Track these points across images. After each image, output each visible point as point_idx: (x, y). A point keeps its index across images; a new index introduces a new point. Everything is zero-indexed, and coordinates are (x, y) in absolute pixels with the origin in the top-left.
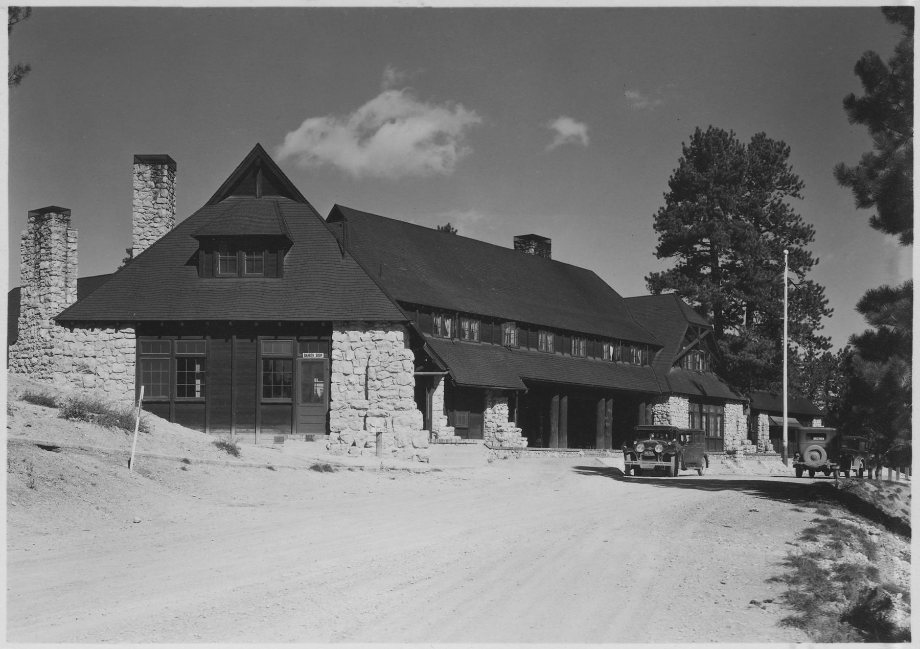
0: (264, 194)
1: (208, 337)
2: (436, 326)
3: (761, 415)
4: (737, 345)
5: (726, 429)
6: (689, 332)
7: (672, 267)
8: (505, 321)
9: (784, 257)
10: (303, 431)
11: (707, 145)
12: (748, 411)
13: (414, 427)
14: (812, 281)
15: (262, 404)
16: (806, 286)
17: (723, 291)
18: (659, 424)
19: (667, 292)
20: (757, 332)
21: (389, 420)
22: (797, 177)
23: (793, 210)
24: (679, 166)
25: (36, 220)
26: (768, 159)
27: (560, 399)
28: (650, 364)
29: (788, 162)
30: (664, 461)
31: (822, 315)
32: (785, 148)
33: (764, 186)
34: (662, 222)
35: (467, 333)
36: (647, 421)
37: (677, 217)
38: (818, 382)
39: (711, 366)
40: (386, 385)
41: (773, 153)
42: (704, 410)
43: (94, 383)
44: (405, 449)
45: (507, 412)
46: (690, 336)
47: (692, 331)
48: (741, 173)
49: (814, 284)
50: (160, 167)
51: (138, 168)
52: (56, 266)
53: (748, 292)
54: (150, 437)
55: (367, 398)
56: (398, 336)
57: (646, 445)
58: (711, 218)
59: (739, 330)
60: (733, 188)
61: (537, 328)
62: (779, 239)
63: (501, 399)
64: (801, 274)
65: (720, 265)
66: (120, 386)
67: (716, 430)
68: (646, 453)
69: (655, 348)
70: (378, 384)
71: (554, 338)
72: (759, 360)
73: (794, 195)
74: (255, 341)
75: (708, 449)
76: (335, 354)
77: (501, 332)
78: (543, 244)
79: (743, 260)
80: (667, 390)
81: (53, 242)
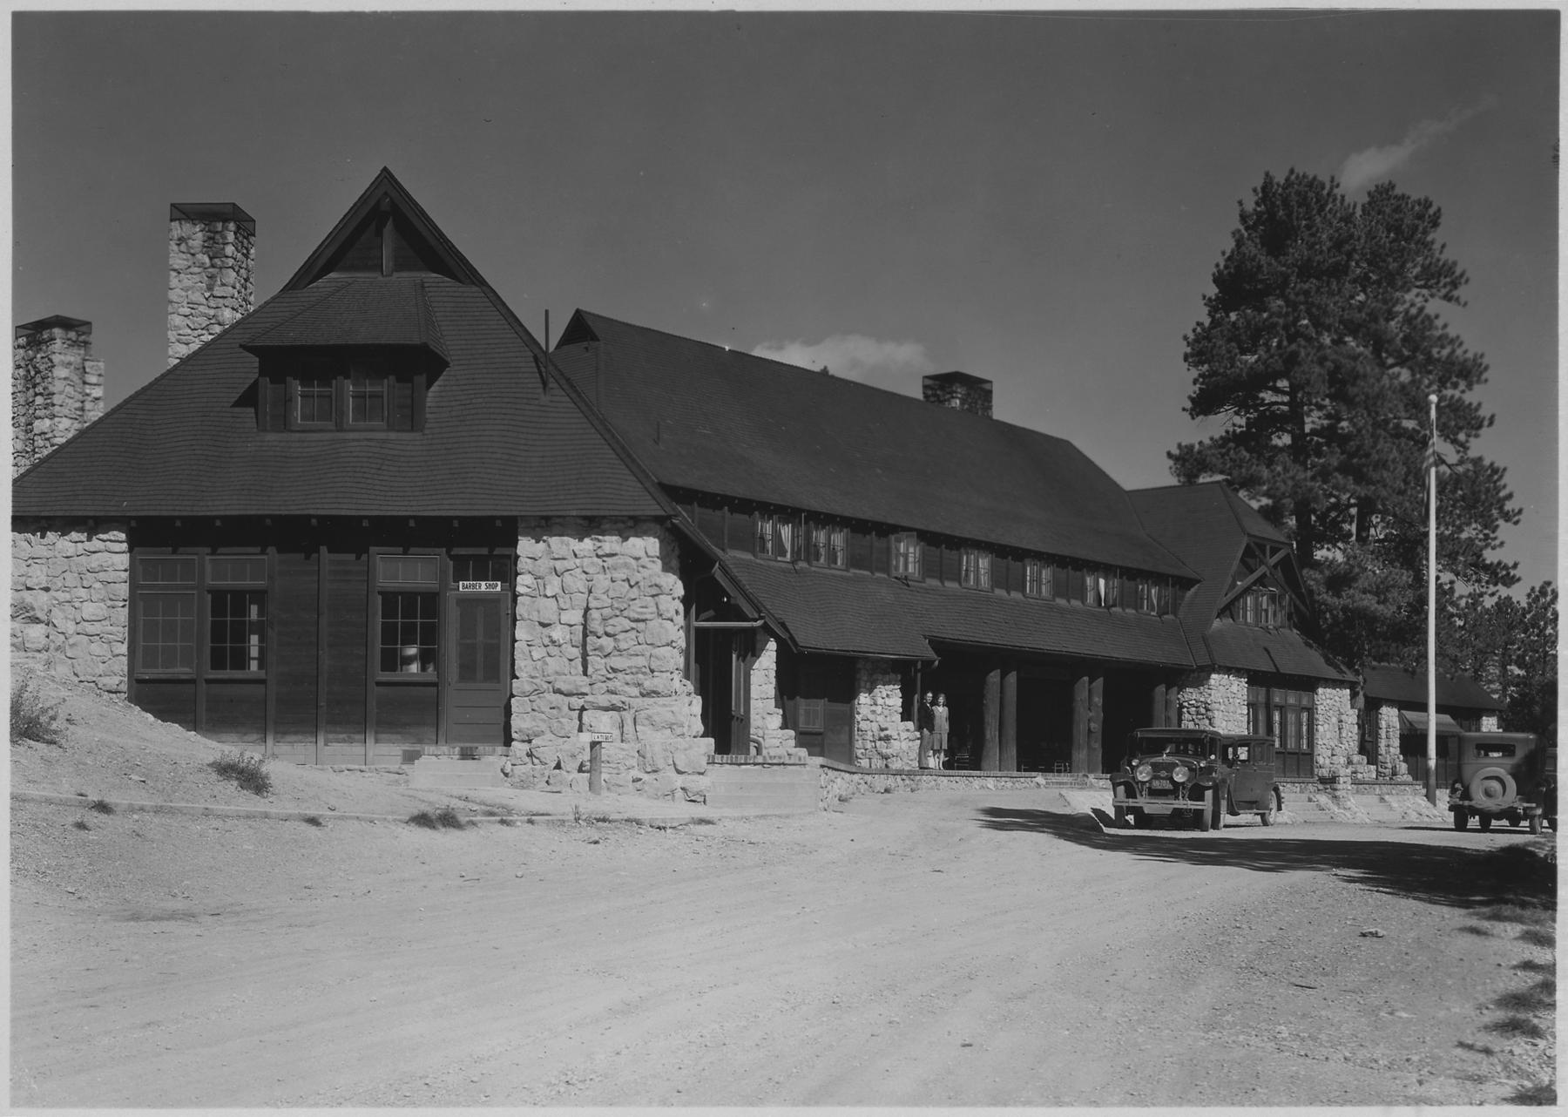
0: (400, 266)
1: (271, 550)
2: (762, 538)
3: (1384, 710)
4: (1339, 580)
5: (1318, 736)
6: (1248, 552)
7: (1219, 433)
8: (895, 529)
9: (1428, 413)
10: (458, 739)
11: (1286, 202)
12: (1361, 700)
13: (679, 731)
14: (1480, 459)
15: (379, 684)
16: (1470, 466)
17: (1313, 478)
18: (1191, 726)
19: (1208, 480)
20: (1377, 555)
21: (628, 716)
22: (1455, 263)
23: (1445, 326)
24: (1233, 244)
25: (28, 343)
26: (1398, 230)
27: (1003, 676)
28: (1175, 614)
29: (1437, 236)
30: (1181, 805)
31: (1501, 522)
32: (1431, 211)
33: (1392, 283)
34: (1200, 350)
35: (822, 551)
36: (1168, 719)
37: (1230, 340)
38: (1481, 657)
39: (1290, 617)
40: (623, 646)
41: (1408, 221)
42: (1277, 700)
43: (44, 641)
44: (661, 774)
45: (899, 702)
46: (1250, 561)
47: (1254, 552)
48: (1349, 255)
49: (1487, 462)
50: (219, 226)
51: (177, 230)
52: (61, 427)
53: (1360, 478)
54: (54, 752)
55: (585, 673)
56: (651, 545)
57: (1156, 767)
58: (1291, 339)
59: (1344, 551)
60: (1334, 286)
61: (959, 544)
62: (1420, 381)
63: (887, 678)
64: (1464, 447)
65: (1307, 430)
66: (96, 648)
67: (1299, 736)
68: (1156, 784)
69: (1185, 583)
70: (607, 643)
71: (992, 564)
72: (1381, 607)
73: (1448, 298)
74: (364, 557)
75: (1284, 772)
76: (523, 583)
77: (888, 549)
78: (978, 390)
79: (1350, 420)
80: (1205, 661)
81: (57, 382)
